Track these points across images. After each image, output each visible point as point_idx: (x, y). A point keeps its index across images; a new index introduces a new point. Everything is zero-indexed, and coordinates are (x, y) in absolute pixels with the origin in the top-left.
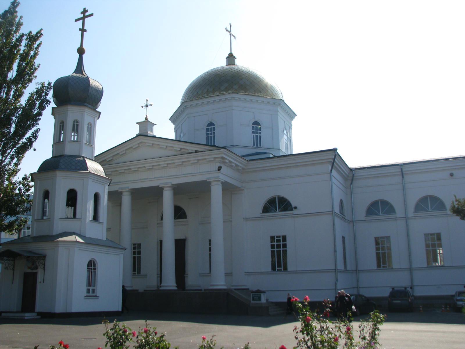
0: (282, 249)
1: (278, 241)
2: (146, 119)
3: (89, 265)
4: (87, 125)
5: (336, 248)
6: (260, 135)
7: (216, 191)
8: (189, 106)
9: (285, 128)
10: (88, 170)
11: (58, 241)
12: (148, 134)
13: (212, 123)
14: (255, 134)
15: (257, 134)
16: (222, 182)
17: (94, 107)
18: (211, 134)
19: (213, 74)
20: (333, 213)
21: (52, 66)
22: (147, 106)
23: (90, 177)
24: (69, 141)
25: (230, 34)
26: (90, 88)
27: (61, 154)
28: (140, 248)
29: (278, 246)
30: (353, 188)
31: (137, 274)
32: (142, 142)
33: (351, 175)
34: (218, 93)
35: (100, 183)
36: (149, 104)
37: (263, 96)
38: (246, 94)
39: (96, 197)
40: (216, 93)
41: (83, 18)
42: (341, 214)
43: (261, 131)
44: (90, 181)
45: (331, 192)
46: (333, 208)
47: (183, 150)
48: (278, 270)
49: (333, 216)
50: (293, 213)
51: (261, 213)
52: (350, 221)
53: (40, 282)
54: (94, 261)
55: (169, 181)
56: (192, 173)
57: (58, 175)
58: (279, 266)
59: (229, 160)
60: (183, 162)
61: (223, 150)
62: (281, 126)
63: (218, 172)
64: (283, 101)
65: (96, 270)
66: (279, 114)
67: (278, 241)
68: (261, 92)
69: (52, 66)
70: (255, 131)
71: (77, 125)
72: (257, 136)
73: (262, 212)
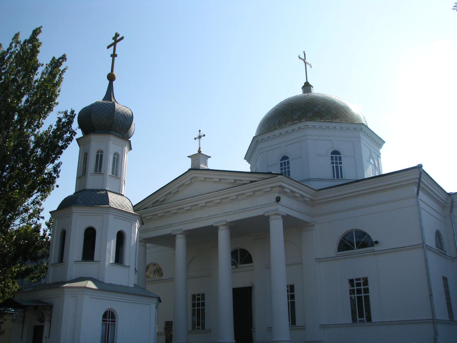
0: (363, 295)
1: (359, 285)
2: (199, 152)
3: (105, 316)
4: (113, 156)
5: (432, 292)
6: (341, 165)
7: (276, 228)
8: (261, 140)
9: (371, 157)
10: (110, 204)
11: (63, 287)
12: (200, 168)
13: (287, 156)
14: (335, 165)
15: (338, 164)
16: (283, 215)
17: (123, 135)
18: (285, 168)
19: (285, 104)
20: (423, 246)
21: (75, 95)
22: (200, 137)
23: (110, 213)
24: (91, 174)
25: (304, 62)
26: (115, 113)
27: (84, 189)
28: (204, 300)
29: (198, 305)
30: (453, 217)
31: (202, 329)
32: (194, 177)
33: (449, 201)
34: (291, 123)
35: (126, 219)
36: (201, 135)
37: (341, 122)
38: (323, 121)
39: (121, 237)
40: (288, 123)
41: (114, 44)
42: (438, 249)
43: (341, 161)
44: (111, 217)
45: (419, 219)
46: (423, 239)
47: (237, 182)
48: (360, 321)
49: (424, 250)
50: (374, 249)
51: (336, 252)
52: (454, 258)
53: (46, 338)
54: (112, 312)
55: (223, 218)
56: (248, 208)
57: (74, 211)
58: (361, 316)
59: (290, 189)
60: (237, 195)
61: (280, 177)
62: (365, 153)
63: (277, 204)
64: (367, 126)
65: (116, 323)
66: (362, 141)
67: (359, 285)
68: (339, 118)
69: (75, 95)
70: (334, 161)
71: (102, 156)
72: (337, 167)
73: (337, 251)
